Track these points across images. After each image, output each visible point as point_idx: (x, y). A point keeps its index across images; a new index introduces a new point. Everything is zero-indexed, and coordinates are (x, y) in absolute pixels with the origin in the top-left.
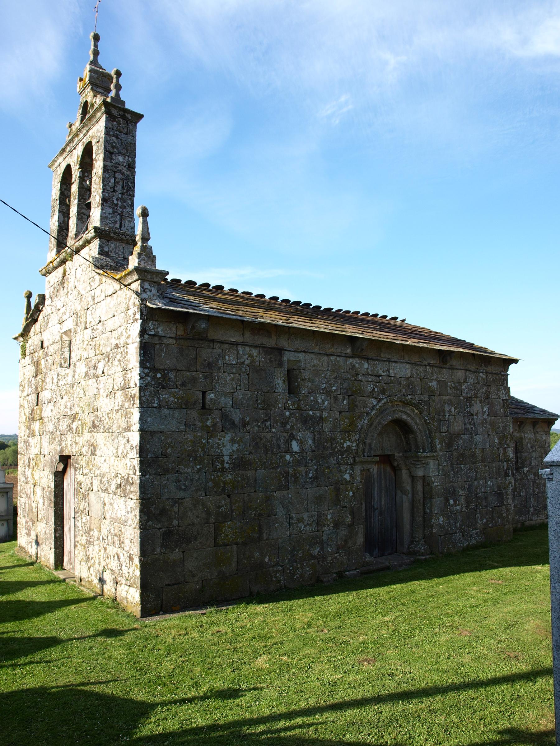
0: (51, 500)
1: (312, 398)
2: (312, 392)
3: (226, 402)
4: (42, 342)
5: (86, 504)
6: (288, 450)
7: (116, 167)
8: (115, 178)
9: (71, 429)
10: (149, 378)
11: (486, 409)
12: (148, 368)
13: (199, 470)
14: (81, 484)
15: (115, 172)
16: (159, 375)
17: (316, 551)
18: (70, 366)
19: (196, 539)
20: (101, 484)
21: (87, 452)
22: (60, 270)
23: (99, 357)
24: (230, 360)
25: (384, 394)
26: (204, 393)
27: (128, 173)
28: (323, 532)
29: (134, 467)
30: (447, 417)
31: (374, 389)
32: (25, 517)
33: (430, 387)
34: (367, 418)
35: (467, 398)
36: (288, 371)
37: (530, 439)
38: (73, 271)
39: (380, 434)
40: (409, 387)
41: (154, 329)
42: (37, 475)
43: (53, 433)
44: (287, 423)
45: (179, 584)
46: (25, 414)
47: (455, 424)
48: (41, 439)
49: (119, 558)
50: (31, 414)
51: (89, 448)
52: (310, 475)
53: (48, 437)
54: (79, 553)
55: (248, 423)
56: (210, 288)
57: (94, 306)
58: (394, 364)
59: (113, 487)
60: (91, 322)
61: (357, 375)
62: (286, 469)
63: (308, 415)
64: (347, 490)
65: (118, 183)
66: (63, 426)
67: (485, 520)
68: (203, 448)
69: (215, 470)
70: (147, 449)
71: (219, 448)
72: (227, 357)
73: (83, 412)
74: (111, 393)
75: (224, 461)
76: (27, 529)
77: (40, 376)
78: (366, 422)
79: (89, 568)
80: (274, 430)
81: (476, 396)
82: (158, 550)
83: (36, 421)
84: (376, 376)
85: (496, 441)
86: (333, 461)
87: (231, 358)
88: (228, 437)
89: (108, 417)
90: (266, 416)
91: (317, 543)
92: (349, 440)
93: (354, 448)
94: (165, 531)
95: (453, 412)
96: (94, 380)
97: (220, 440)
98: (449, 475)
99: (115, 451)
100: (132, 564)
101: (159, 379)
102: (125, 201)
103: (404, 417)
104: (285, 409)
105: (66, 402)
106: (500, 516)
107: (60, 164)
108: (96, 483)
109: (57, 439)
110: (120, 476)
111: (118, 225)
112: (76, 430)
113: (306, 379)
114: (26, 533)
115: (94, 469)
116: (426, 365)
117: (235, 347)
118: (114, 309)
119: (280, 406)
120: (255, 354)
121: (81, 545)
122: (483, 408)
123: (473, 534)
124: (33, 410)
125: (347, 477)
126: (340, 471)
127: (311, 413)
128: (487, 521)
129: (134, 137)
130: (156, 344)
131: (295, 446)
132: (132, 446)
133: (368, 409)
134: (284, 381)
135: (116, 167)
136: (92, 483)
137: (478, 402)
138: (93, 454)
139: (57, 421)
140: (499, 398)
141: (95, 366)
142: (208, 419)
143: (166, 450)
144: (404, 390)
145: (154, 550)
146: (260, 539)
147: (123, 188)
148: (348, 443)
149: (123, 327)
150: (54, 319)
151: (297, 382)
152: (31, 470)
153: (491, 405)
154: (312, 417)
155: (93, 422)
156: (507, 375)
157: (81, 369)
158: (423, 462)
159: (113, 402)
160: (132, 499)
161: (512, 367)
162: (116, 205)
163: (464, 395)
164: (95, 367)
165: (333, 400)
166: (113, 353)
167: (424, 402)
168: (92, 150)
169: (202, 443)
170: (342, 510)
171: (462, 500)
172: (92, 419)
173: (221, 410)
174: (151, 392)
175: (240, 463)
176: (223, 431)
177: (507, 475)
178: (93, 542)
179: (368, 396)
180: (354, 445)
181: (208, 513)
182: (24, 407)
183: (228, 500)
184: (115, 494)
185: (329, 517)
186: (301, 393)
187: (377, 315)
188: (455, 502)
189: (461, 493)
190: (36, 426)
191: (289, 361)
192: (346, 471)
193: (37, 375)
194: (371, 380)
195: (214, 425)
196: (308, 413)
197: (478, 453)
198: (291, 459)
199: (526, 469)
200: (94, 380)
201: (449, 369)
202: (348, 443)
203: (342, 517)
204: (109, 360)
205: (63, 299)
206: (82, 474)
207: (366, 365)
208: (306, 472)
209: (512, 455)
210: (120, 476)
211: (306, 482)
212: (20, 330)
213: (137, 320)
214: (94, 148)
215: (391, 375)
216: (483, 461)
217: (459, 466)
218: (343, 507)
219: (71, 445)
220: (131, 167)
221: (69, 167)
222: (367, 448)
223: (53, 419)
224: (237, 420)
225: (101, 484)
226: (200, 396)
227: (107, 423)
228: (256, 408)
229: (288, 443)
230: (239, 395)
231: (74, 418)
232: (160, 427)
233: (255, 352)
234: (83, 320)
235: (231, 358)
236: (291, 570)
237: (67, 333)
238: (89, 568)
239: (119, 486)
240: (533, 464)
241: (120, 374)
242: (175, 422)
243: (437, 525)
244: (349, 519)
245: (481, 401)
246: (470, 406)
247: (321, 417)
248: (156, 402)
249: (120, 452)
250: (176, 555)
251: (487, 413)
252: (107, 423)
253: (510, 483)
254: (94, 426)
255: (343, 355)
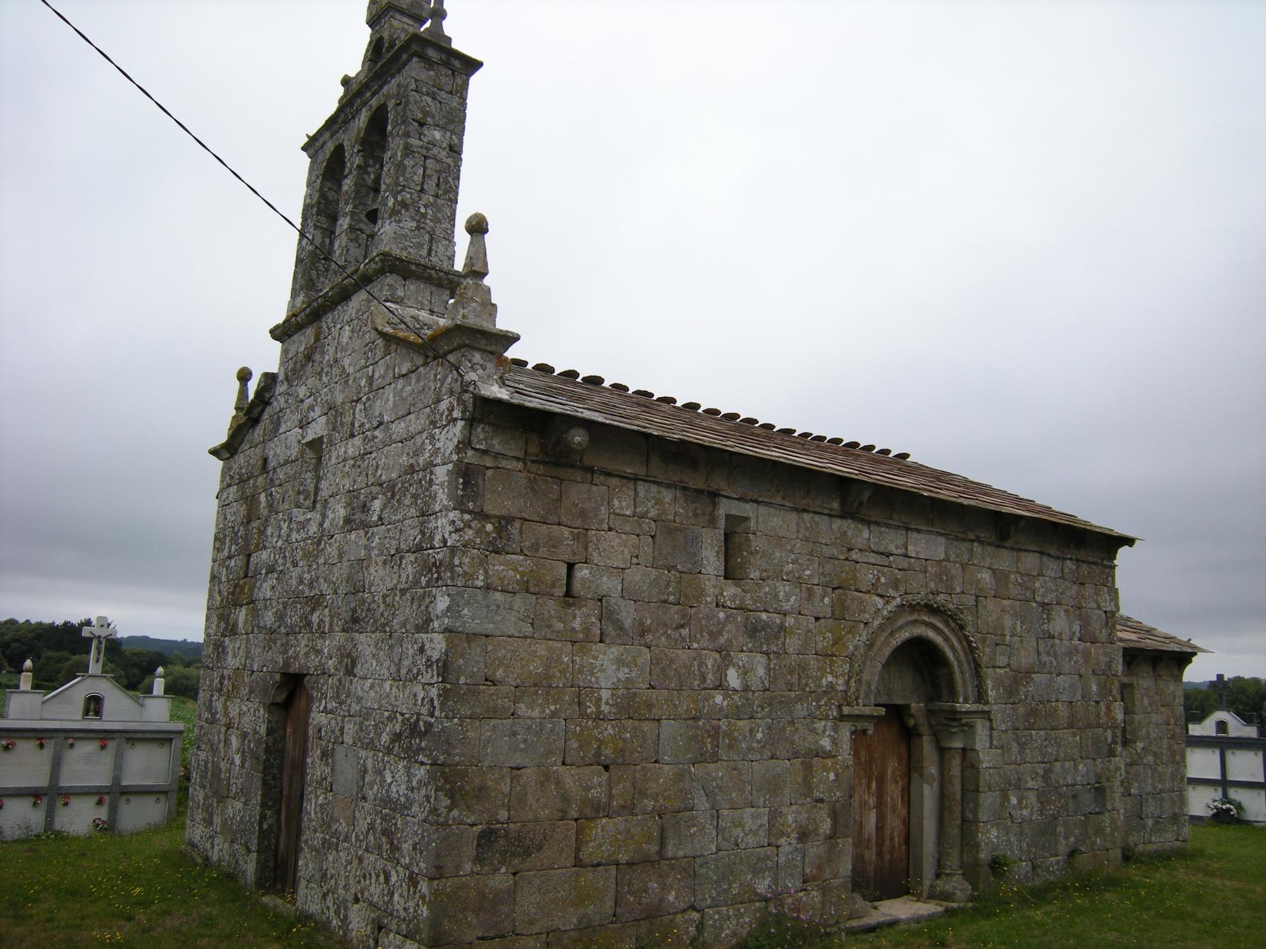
0: (257, 758)
1: (767, 589)
2: (768, 578)
3: (609, 585)
4: (265, 460)
5: (328, 770)
6: (721, 686)
7: (428, 149)
8: (425, 169)
9: (309, 624)
10: (471, 532)
11: (1076, 628)
12: (470, 512)
13: (554, 715)
14: (319, 731)
15: (426, 158)
16: (489, 527)
17: (762, 886)
18: (314, 507)
19: (539, 849)
20: (361, 730)
21: (336, 669)
22: (310, 332)
23: (375, 489)
24: (621, 508)
25: (896, 588)
26: (571, 567)
27: (449, 161)
28: (778, 847)
29: (432, 700)
30: (1008, 638)
31: (879, 579)
32: (203, 787)
33: (978, 581)
34: (865, 633)
35: (1043, 605)
36: (726, 535)
37: (1147, 689)
38: (335, 332)
39: (887, 665)
40: (941, 580)
41: (485, 439)
42: (234, 711)
43: (272, 631)
44: (720, 633)
45: (502, 937)
46: (220, 592)
47: (1022, 653)
48: (248, 640)
49: (387, 879)
50: (233, 593)
51: (340, 662)
52: (759, 736)
53: (261, 637)
54: (307, 865)
55: (649, 631)
56: (579, 380)
57: (371, 396)
58: (915, 534)
59: (385, 738)
60: (362, 425)
61: (850, 550)
62: (714, 722)
63: (759, 620)
64: (825, 769)
65: (430, 176)
66: (292, 618)
67: (1072, 839)
68: (563, 672)
69: (583, 715)
70: (460, 667)
71: (592, 674)
72: (616, 502)
73: (335, 592)
74: (394, 558)
75: (600, 699)
76: (207, 811)
77: (255, 524)
78: (864, 638)
79: (325, 896)
80: (695, 645)
81: (1059, 603)
82: (468, 867)
83: (241, 606)
84: (882, 554)
85: (1094, 688)
86: (800, 710)
87: (624, 504)
88: (614, 651)
89: (384, 602)
90: (684, 616)
91: (768, 869)
92: (831, 673)
93: (840, 688)
94: (483, 831)
95: (1019, 629)
96: (362, 533)
97: (596, 658)
98: (1009, 749)
99: (393, 669)
100: (415, 893)
101: (488, 534)
102: (439, 210)
103: (931, 634)
104: (717, 605)
105: (303, 573)
106: (1099, 831)
107: (324, 143)
108: (350, 728)
109: (279, 642)
110: (400, 718)
111: (424, 252)
112: (319, 627)
113: (757, 552)
114: (204, 819)
115: (348, 701)
116: (972, 541)
117: (631, 484)
118: (410, 400)
119: (709, 599)
120: (667, 500)
121: (312, 849)
122: (1070, 627)
123: (1051, 865)
124: (236, 586)
125: (826, 743)
126: (814, 731)
127: (764, 616)
128: (1077, 841)
129: (463, 99)
130: (488, 468)
131: (733, 679)
132: (428, 660)
133: (867, 616)
134: (718, 552)
135: (428, 149)
136: (342, 729)
137: (1062, 613)
138: (350, 672)
139: (281, 607)
140: (1099, 608)
141: (364, 506)
142: (575, 617)
143: (494, 673)
144: (932, 585)
145: (458, 868)
146: (661, 854)
147: (438, 185)
148: (830, 678)
149: (425, 435)
150: (290, 419)
151: (743, 557)
152: (222, 699)
153: (1085, 621)
154: (766, 626)
155: (354, 611)
156: (1114, 567)
157: (339, 511)
158: (964, 721)
159: (396, 576)
160: (422, 763)
161: (1123, 552)
162: (424, 216)
163: (1038, 599)
164: (365, 508)
165: (805, 595)
166: (403, 483)
167: (968, 609)
168: (387, 119)
169: (562, 663)
170: (815, 807)
171: (1032, 798)
172: (353, 605)
173: (600, 600)
174: (473, 558)
175: (630, 707)
176: (601, 641)
177: (1112, 754)
178: (337, 844)
179: (869, 592)
180: (841, 681)
181: (565, 799)
182: (220, 579)
183: (605, 776)
184: (389, 751)
185: (790, 818)
186: (747, 578)
187: (872, 447)
188: (1020, 802)
189: (1030, 784)
190: (242, 615)
191: (728, 516)
192: (824, 732)
193: (249, 522)
194: (873, 561)
195: (587, 630)
196: (759, 618)
197: (1063, 710)
198: (725, 703)
199: (1140, 745)
200: (362, 533)
201: (1012, 549)
202: (830, 678)
203: (814, 820)
204: (393, 496)
205: (310, 382)
206: (325, 711)
207: (866, 534)
208: (751, 731)
209: (1120, 717)
210: (400, 718)
211: (750, 749)
212: (222, 437)
213: (456, 419)
214: (391, 116)
215: (910, 554)
216: (1071, 726)
217: (1027, 732)
218: (817, 801)
219: (307, 654)
220: (455, 151)
221: (340, 149)
222: (863, 688)
223: (274, 603)
224: (628, 623)
225: (361, 730)
226: (563, 570)
227: (382, 615)
228: (665, 601)
229: (721, 671)
230: (635, 576)
231: (316, 602)
232: (486, 626)
233: (667, 496)
234: (347, 419)
235: (624, 504)
236: (715, 921)
237: (316, 445)
238: (325, 896)
239: (397, 737)
240: (1153, 735)
241: (415, 522)
242: (513, 619)
243: (986, 844)
244: (826, 826)
245: (1067, 611)
246: (1049, 620)
247: (782, 627)
248: (481, 578)
249: (403, 671)
250: (500, 880)
251: (1078, 634)
252: (382, 615)
253: (1118, 769)
254: (355, 620)
255: (826, 512)
